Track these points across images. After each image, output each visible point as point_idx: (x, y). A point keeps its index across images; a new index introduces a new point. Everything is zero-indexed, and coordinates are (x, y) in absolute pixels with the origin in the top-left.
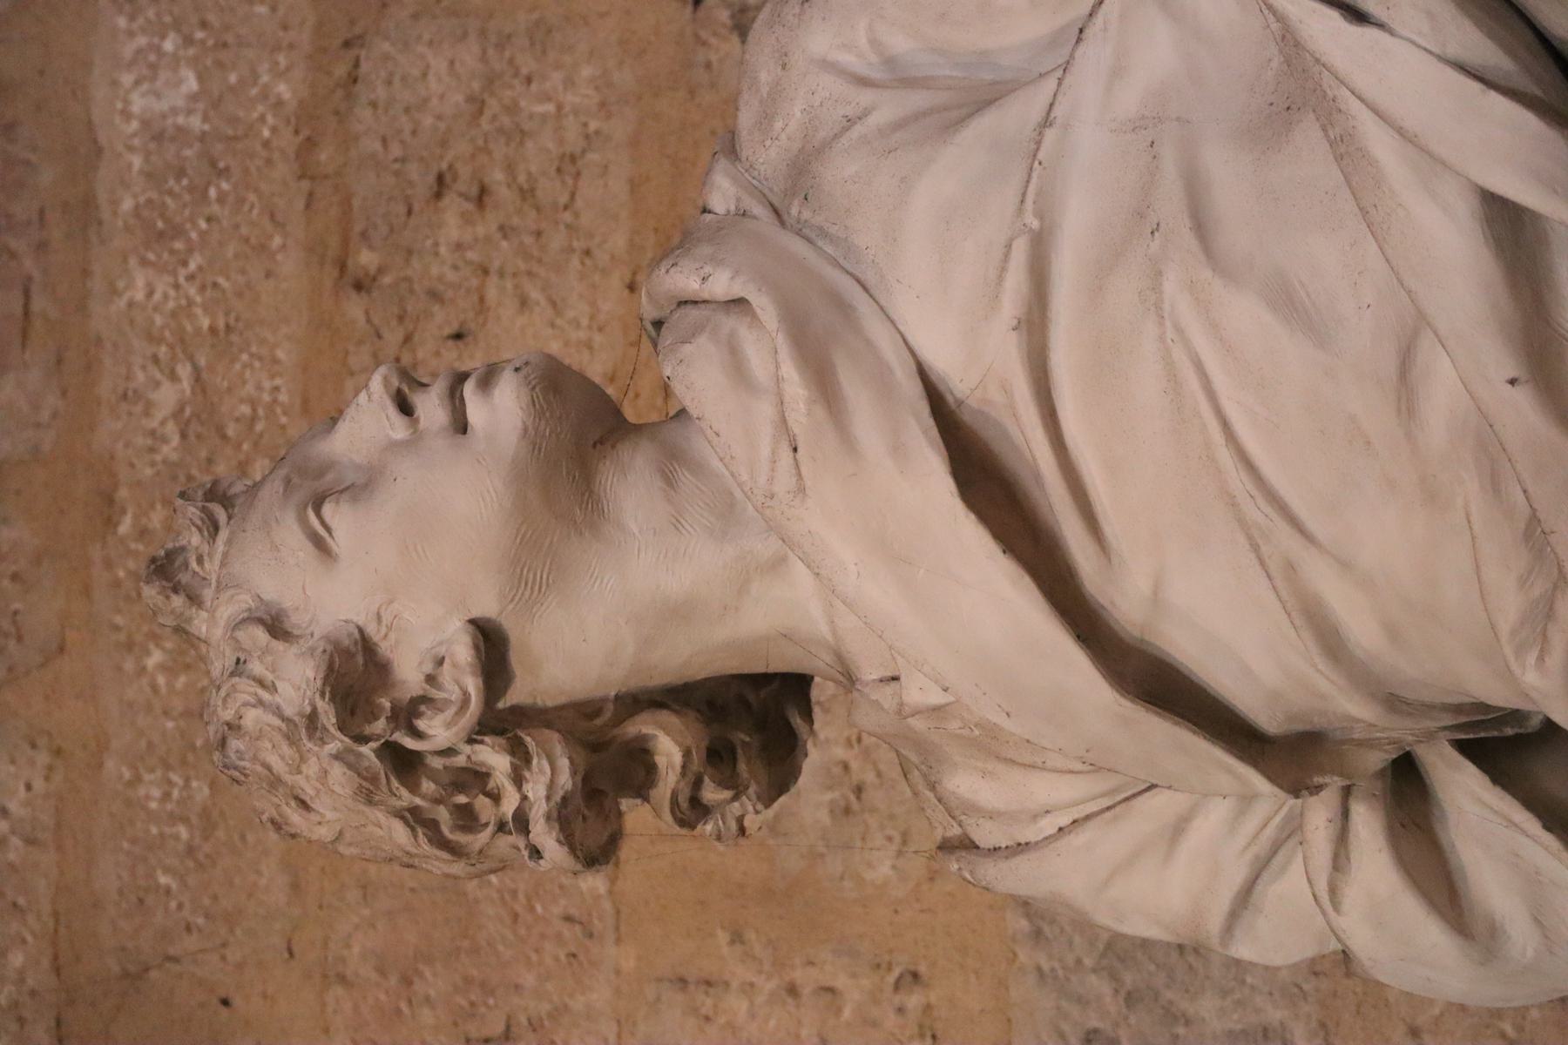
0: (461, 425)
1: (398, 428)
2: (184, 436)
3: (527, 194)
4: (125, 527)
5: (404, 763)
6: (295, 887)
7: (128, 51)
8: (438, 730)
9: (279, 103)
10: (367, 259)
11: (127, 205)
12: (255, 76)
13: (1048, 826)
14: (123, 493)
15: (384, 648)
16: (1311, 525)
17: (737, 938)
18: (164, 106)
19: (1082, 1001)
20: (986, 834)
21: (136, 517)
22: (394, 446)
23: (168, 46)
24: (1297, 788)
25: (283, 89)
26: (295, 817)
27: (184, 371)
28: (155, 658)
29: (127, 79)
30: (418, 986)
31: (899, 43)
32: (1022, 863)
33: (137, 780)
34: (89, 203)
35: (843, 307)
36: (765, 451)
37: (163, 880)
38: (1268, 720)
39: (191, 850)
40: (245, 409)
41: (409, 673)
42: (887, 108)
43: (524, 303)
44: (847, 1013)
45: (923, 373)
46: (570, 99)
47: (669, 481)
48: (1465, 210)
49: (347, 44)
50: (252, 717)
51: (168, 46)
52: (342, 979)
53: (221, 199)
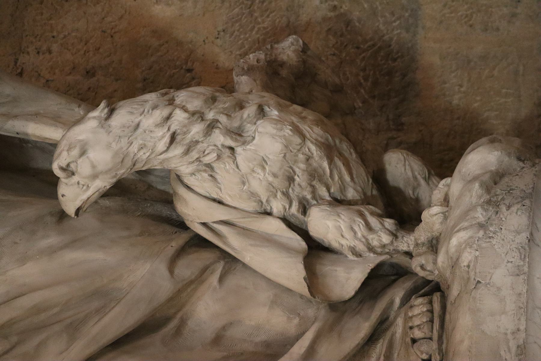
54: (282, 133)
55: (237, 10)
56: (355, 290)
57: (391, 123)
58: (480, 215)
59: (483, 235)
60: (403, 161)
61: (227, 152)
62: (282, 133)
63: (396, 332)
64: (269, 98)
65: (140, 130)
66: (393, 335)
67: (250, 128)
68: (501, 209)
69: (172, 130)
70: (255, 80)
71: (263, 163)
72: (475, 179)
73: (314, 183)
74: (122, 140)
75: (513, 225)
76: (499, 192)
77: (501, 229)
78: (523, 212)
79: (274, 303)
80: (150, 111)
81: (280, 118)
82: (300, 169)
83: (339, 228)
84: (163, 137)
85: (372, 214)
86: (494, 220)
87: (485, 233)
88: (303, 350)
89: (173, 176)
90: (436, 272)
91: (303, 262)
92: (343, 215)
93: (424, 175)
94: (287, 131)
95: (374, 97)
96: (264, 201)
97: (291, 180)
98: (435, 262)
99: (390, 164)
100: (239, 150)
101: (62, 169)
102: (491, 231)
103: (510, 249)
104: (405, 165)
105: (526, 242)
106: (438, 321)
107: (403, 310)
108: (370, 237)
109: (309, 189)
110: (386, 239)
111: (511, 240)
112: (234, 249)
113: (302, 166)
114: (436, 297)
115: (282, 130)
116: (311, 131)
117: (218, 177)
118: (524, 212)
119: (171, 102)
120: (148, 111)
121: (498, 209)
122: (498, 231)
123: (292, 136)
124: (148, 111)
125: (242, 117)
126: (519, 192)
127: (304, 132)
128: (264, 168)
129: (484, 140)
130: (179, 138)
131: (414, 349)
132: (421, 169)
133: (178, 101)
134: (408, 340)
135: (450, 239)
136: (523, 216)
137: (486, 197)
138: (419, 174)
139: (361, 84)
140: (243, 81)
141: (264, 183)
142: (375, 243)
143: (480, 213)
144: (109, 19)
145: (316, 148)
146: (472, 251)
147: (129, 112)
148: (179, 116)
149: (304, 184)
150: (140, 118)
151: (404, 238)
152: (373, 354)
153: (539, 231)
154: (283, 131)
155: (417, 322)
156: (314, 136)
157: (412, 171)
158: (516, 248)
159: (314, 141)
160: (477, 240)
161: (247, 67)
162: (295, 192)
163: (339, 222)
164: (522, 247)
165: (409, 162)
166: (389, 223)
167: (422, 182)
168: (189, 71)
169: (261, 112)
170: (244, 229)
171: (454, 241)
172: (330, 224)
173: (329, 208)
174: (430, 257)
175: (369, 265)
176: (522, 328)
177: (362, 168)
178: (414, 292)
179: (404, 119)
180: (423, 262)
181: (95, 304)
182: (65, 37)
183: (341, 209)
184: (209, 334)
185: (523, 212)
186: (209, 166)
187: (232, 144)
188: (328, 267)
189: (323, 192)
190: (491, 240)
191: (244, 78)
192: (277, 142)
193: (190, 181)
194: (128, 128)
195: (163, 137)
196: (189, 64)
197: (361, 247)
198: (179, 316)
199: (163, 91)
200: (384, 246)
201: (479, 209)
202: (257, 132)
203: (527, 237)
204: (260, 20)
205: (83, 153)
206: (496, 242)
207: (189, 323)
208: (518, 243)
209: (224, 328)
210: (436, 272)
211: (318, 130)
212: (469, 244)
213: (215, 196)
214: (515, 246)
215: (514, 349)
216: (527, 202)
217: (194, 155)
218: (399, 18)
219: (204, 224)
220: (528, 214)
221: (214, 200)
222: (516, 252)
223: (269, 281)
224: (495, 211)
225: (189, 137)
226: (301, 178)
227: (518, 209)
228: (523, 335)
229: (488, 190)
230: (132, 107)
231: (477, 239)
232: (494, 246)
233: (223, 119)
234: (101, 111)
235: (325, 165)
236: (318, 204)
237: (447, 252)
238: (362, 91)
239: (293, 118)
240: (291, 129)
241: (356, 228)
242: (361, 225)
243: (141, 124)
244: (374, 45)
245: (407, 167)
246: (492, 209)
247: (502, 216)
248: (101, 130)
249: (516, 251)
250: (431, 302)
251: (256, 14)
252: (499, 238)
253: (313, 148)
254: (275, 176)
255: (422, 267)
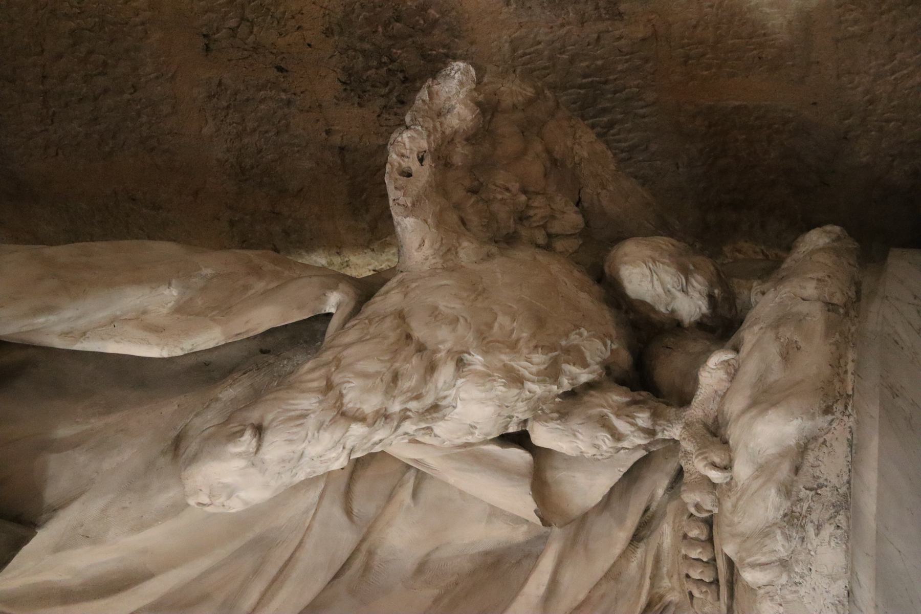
54: (493, 394)
56: (602, 495)
57: (603, 11)
59: (787, 581)
60: (649, 276)
62: (493, 394)
63: (663, 543)
65: (305, 459)
68: (808, 532)
70: (425, 221)
74: (283, 476)
75: (826, 566)
77: (811, 570)
78: (838, 543)
80: (316, 434)
81: (488, 367)
86: (800, 553)
87: (789, 576)
91: (531, 493)
92: (581, 434)
93: (681, 286)
99: (630, 282)
102: (796, 573)
103: (825, 606)
104: (652, 281)
105: (844, 594)
106: (726, 590)
111: (824, 590)
112: (432, 469)
115: (492, 389)
116: (529, 364)
118: (840, 542)
120: (314, 435)
121: (804, 534)
122: (807, 573)
123: (507, 392)
124: (314, 435)
125: (436, 387)
126: (830, 491)
127: (521, 373)
131: (694, 608)
132: (676, 279)
136: (839, 549)
137: (786, 505)
138: (674, 287)
140: (409, 226)
143: (780, 544)
145: (538, 385)
146: (774, 606)
147: (285, 440)
150: (304, 445)
151: (665, 432)
152: (632, 558)
153: (861, 587)
154: (494, 390)
156: (534, 369)
157: (662, 284)
158: (832, 604)
159: (536, 378)
160: (780, 589)
161: (411, 203)
163: (576, 442)
164: (839, 602)
165: (658, 276)
167: (679, 295)
173: (560, 425)
175: (619, 469)
177: (596, 340)
180: (699, 500)
184: (410, 564)
185: (838, 543)
188: (562, 472)
190: (798, 588)
192: (488, 406)
194: (289, 462)
202: (458, 399)
203: (846, 587)
206: (806, 592)
207: (379, 551)
208: (833, 596)
209: (428, 555)
214: (829, 601)
220: (844, 546)
222: (832, 609)
224: (800, 537)
227: (831, 535)
230: (289, 433)
231: (780, 587)
232: (803, 598)
239: (504, 358)
240: (504, 383)
242: (605, 439)
243: (306, 452)
245: (656, 283)
246: (796, 535)
247: (810, 547)
248: (252, 470)
249: (833, 609)
252: (808, 586)
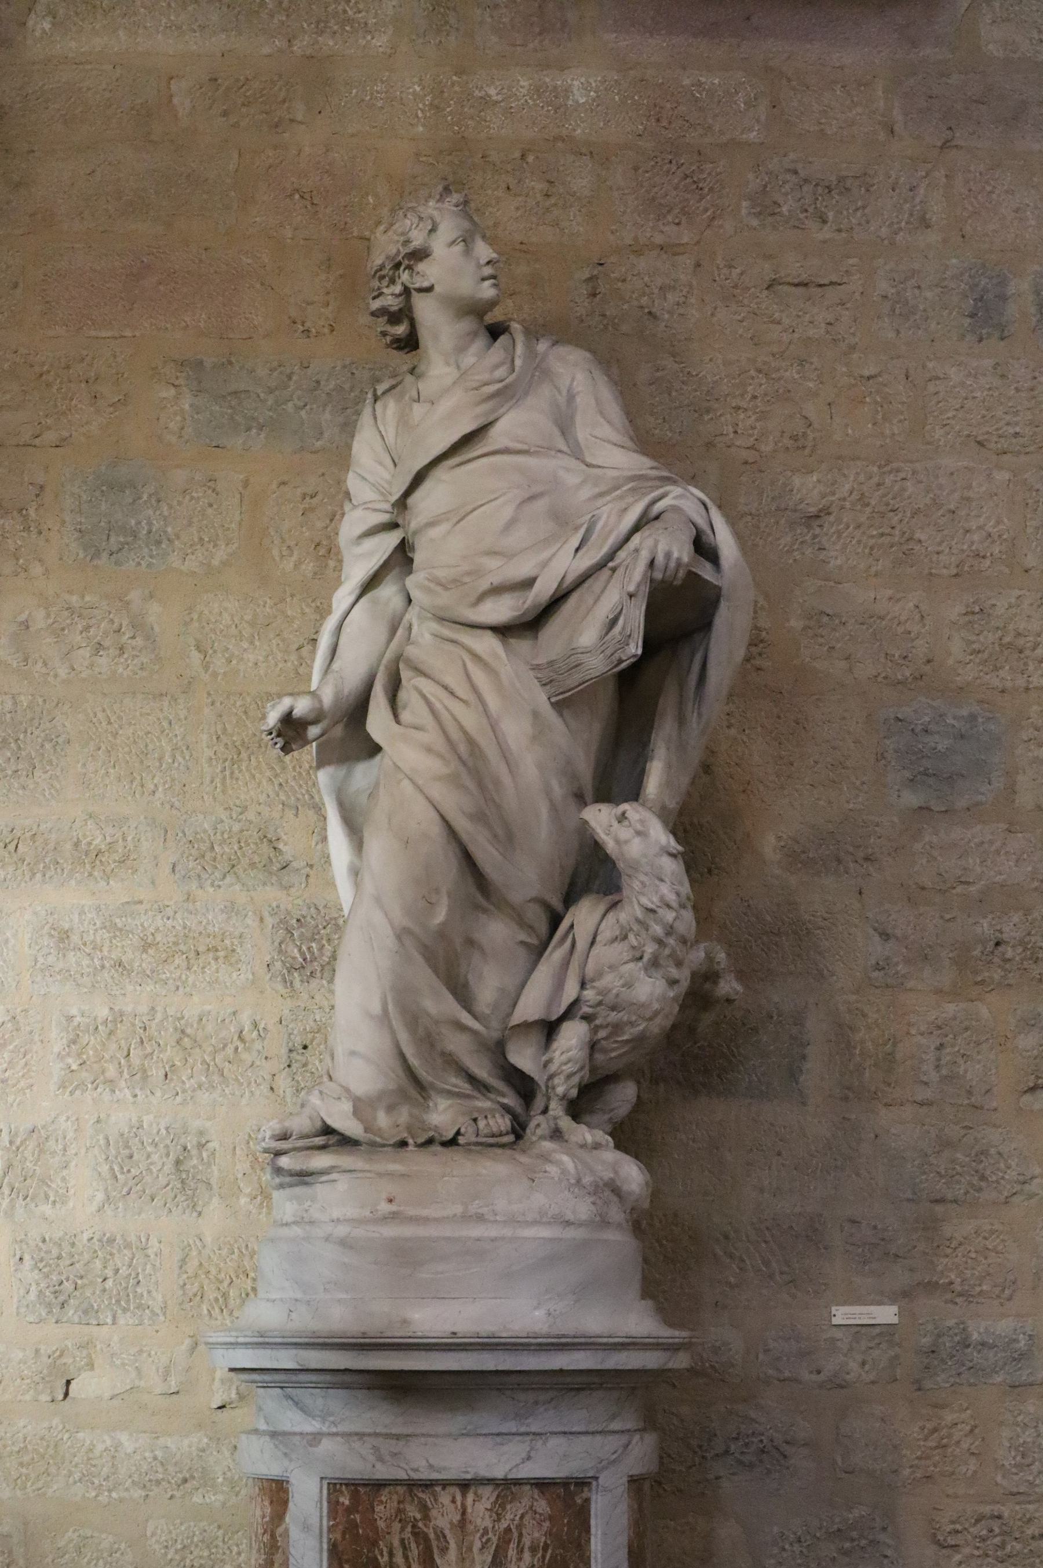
0: (483, 279)
1: (483, 261)
2: (481, 98)
3: (548, 210)
4: (454, 78)
5: (397, 266)
6: (353, 136)
7: (591, 81)
8: (405, 276)
9: (575, 130)
10: (531, 158)
11: (547, 80)
12: (583, 122)
13: (382, 428)
14: (465, 77)
15: (426, 261)
16: (458, 526)
17: (341, 276)
18: (575, 92)
19: (327, 380)
20: (379, 405)
21: (458, 82)
22: (478, 259)
23: (592, 93)
24: (393, 505)
25: (579, 131)
26: (382, 228)
27: (500, 98)
28: (418, 89)
29: (583, 80)
30: (326, 175)
31: (578, 399)
32: (372, 421)
33: (382, 82)
34: (548, 66)
35: (512, 397)
36: (477, 378)
37: (354, 91)
38: (410, 501)
39: (363, 100)
40: (488, 118)
41: (421, 267)
42: (562, 400)
43: (517, 209)
44: (322, 310)
45: (496, 420)
46: (574, 223)
47: (468, 334)
48: (532, 573)
49: (591, 153)
50: (408, 222)
51: (592, 93)
52: (328, 151)
53: (548, 111)
55: (769, 918)
58: (587, 1180)
61: (638, 955)
64: (685, 984)
65: (657, 882)
66: (477, 1098)
67: (658, 974)
69: (659, 911)
71: (628, 985)
72: (616, 1172)
73: (610, 1028)
76: (606, 1194)
79: (502, 990)
82: (623, 1016)
83: (568, 1051)
84: (652, 903)
85: (582, 1077)
88: (464, 1021)
89: (615, 897)
90: (534, 1138)
94: (656, 1006)
95: (683, 1056)
96: (594, 984)
97: (613, 1008)
98: (542, 1138)
100: (640, 964)
101: (624, 813)
107: (497, 1107)
108: (562, 1077)
109: (605, 1023)
110: (560, 1090)
113: (625, 1018)
114: (511, 1138)
117: (616, 944)
119: (683, 906)
128: (623, 986)
129: (648, 1176)
130: (652, 915)
133: (683, 912)
134: (475, 1115)
135: (567, 1154)
139: (695, 1043)
141: (610, 986)
142: (556, 1081)
144: (761, 788)
148: (669, 916)
149: (609, 1019)
155: (491, 1122)
162: (602, 1011)
166: (574, 1093)
168: (710, 871)
169: (673, 982)
170: (568, 963)
171: (565, 1158)
172: (574, 1042)
174: (547, 1132)
176: (498, 1218)
178: (515, 1117)
179: (662, 1085)
181: (500, 832)
182: (744, 743)
183: (587, 1051)
184: (477, 936)
186: (625, 937)
187: (646, 958)
189: (602, 1034)
191: (702, 954)
193: (611, 917)
195: (652, 903)
196: (716, 871)
197: (553, 1068)
198: (491, 907)
199: (692, 897)
200: (554, 1088)
201: (592, 1179)
204: (759, 941)
205: (638, 833)
207: (485, 916)
210: (534, 1138)
211: (656, 1030)
212: (564, 1171)
213: (598, 938)
215: (480, 1211)
216: (598, 1219)
217: (636, 927)
218: (759, 1081)
219: (572, 926)
221: (594, 938)
223: (523, 985)
225: (652, 923)
226: (613, 1017)
228: (492, 1219)
229: (606, 1185)
233: (667, 951)
234: (673, 845)
235: (625, 1038)
236: (590, 1030)
237: (554, 1151)
238: (689, 1045)
241: (569, 1065)
244: (734, 1056)
250: (507, 1133)
251: (765, 938)
253: (641, 1028)
254: (617, 995)
255: (538, 1125)
